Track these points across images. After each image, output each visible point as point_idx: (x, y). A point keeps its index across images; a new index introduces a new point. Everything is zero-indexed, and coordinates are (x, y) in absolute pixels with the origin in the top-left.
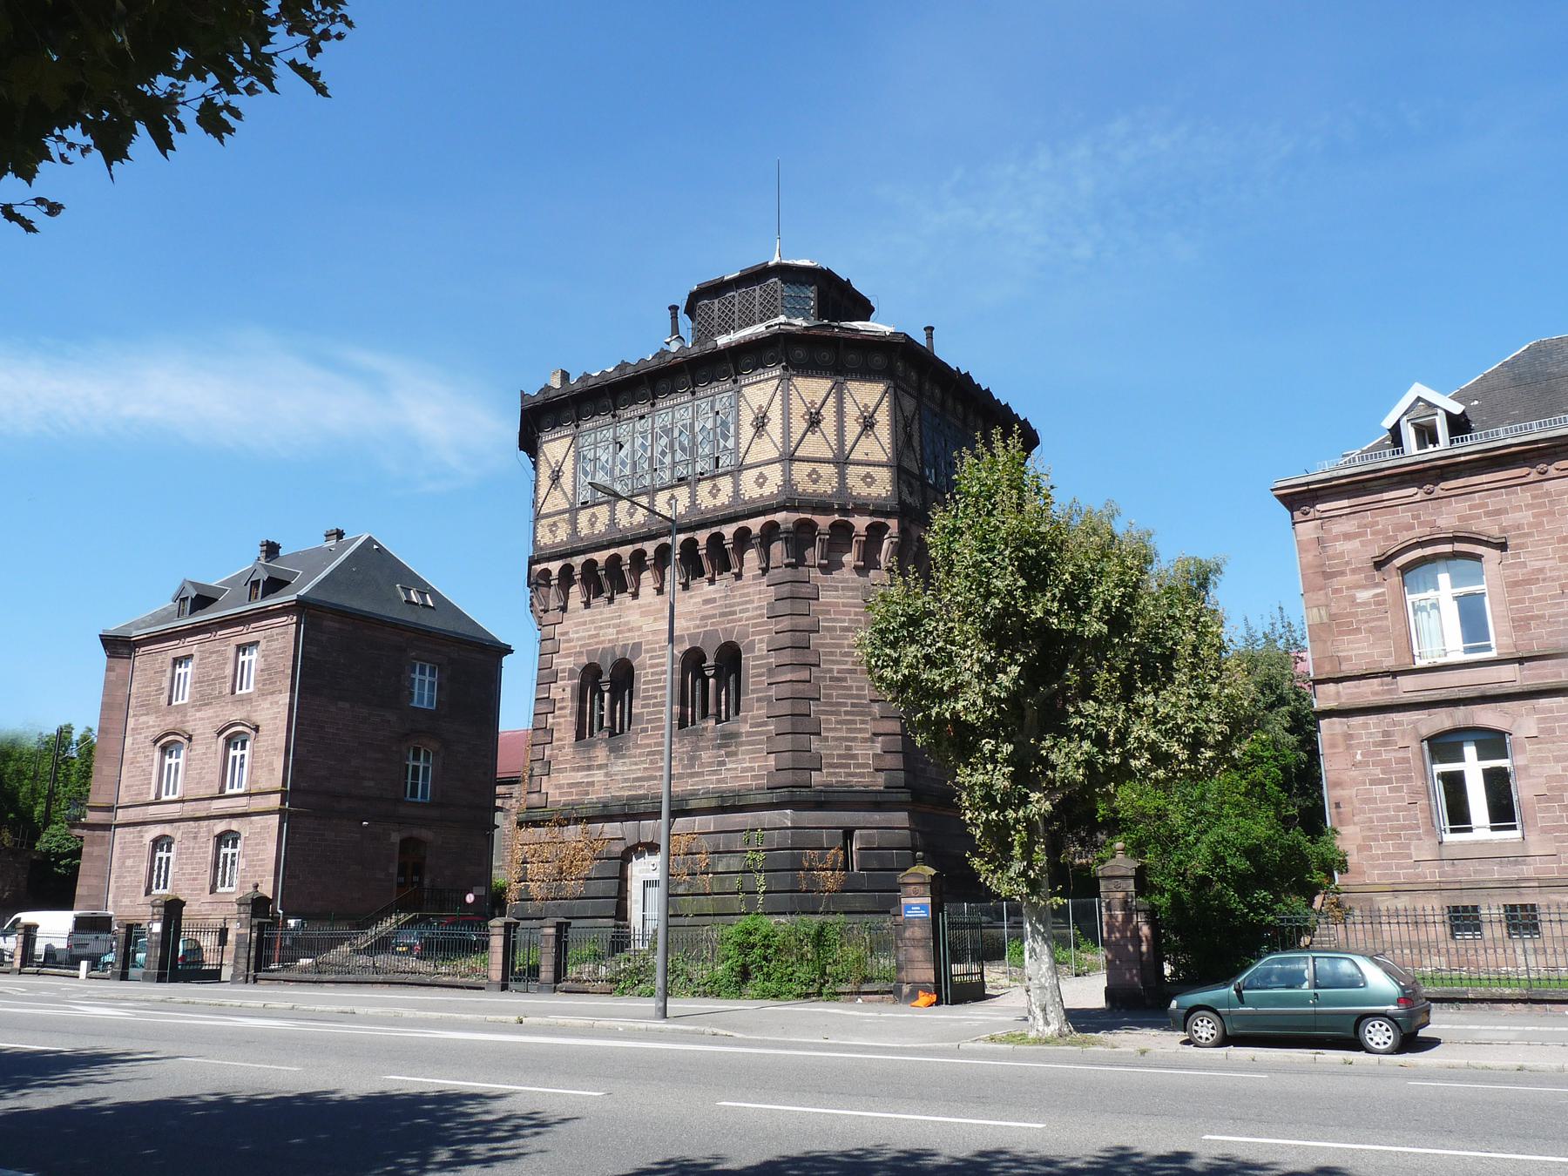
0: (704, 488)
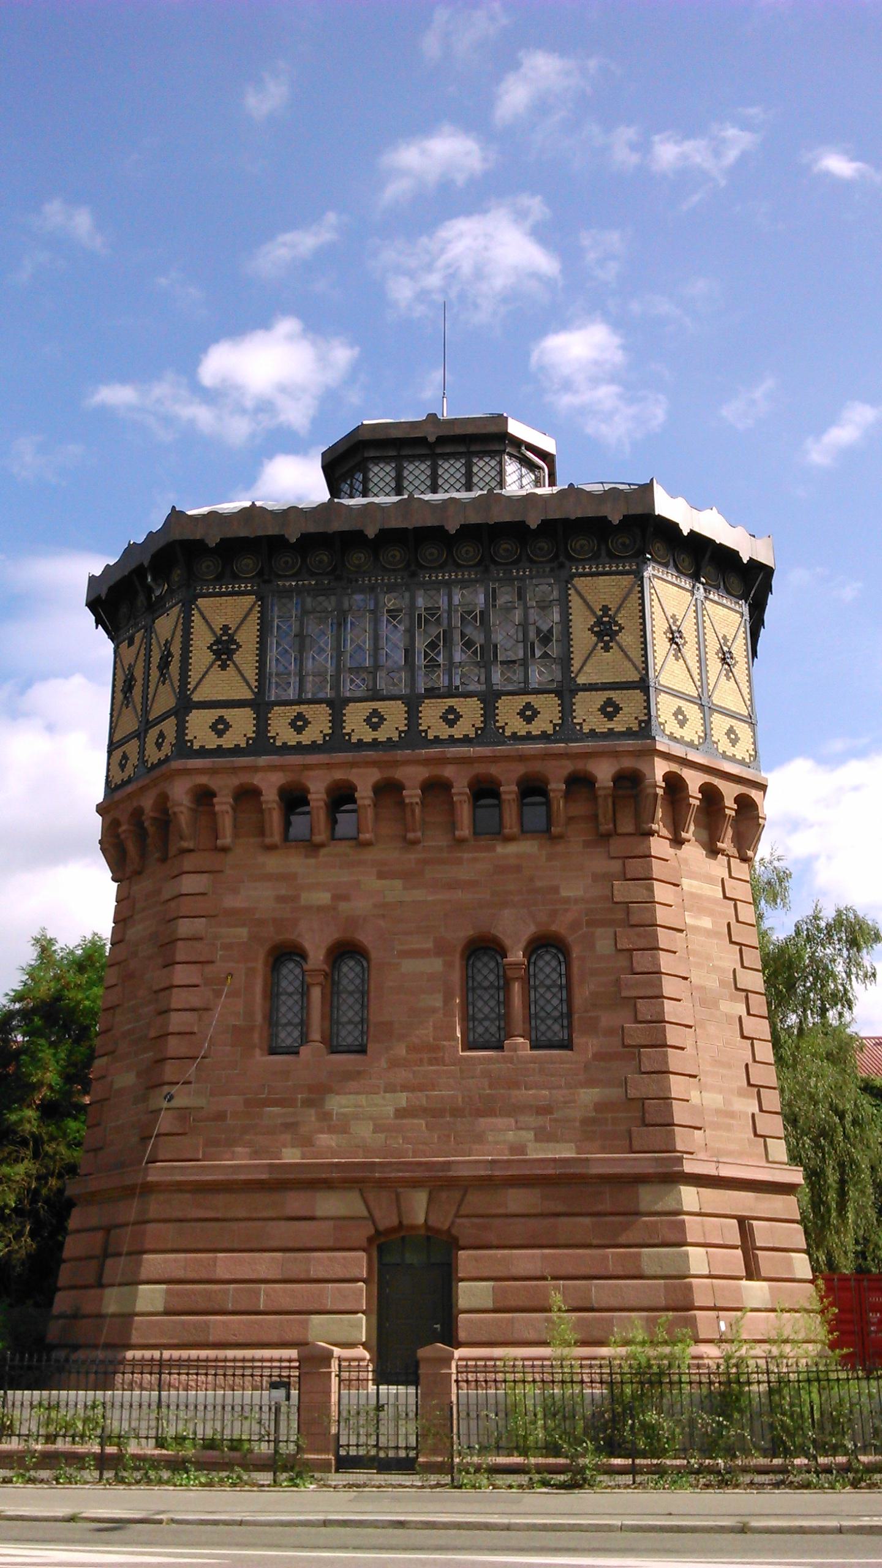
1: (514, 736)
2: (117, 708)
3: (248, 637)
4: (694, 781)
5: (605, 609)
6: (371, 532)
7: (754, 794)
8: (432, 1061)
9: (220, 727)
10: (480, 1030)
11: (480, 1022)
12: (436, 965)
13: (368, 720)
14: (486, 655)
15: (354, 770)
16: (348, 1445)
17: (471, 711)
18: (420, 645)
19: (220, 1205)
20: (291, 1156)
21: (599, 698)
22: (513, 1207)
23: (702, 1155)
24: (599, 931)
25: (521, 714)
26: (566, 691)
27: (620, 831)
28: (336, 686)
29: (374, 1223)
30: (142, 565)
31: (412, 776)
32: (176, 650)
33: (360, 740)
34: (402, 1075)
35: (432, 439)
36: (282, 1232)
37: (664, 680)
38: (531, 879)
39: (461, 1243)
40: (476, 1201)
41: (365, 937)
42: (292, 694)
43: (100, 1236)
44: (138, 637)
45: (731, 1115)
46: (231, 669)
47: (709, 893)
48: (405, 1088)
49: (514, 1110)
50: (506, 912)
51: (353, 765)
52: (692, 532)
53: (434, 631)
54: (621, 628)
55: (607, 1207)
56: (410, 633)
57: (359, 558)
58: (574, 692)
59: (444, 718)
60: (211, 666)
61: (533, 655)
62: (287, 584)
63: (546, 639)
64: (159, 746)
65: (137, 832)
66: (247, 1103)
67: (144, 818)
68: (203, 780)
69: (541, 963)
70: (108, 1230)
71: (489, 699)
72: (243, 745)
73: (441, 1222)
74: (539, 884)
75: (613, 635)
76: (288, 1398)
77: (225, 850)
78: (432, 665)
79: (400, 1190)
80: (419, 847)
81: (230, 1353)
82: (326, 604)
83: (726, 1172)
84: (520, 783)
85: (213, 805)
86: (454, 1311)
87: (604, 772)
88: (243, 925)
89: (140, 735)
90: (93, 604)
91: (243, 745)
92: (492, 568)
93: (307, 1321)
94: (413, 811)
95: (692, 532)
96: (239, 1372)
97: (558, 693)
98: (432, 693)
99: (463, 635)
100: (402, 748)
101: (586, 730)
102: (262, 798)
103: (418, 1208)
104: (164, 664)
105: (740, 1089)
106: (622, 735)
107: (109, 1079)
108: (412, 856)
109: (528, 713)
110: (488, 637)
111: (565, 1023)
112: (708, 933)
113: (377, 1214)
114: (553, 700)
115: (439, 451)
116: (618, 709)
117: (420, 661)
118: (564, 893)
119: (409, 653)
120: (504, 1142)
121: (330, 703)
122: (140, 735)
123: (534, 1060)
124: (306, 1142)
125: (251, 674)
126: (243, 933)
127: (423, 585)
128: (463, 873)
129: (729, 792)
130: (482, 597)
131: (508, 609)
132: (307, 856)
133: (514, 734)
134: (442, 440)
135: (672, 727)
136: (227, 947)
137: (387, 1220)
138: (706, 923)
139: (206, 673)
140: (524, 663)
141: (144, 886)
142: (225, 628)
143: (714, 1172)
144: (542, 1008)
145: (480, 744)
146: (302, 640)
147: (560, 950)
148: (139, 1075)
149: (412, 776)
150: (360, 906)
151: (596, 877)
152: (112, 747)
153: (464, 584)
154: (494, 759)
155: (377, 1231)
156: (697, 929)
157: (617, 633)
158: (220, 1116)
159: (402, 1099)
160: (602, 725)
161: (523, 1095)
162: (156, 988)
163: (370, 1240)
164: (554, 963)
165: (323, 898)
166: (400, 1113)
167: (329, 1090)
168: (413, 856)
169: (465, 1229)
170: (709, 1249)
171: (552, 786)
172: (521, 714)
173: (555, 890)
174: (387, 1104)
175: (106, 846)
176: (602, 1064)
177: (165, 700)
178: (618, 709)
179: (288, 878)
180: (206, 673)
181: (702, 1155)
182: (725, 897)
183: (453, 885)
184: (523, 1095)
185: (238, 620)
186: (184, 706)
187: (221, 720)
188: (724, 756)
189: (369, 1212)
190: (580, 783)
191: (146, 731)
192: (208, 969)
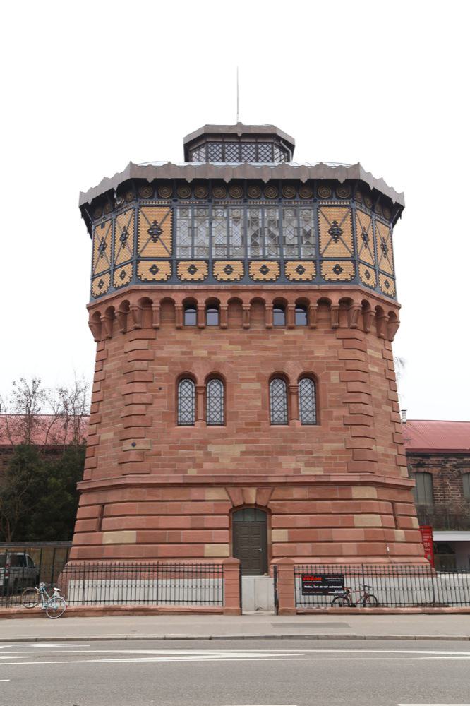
1: (294, 281)
2: (96, 258)
3: (166, 227)
4: (373, 304)
5: (335, 223)
6: (227, 180)
7: (395, 311)
8: (257, 430)
9: (154, 270)
10: (276, 416)
11: (276, 412)
12: (257, 386)
13: (225, 270)
14: (280, 242)
15: (219, 293)
16: (114, 601)
17: (274, 268)
18: (249, 234)
19: (160, 494)
20: (192, 472)
21: (333, 264)
22: (296, 497)
23: (377, 474)
24: (332, 372)
25: (297, 270)
26: (318, 260)
27: (341, 326)
28: (210, 253)
30: (113, 189)
31: (247, 298)
32: (131, 231)
33: (222, 279)
34: (244, 436)
35: (240, 135)
36: (190, 507)
37: (362, 257)
38: (301, 347)
39: (272, 512)
40: (279, 493)
41: (224, 372)
43: (98, 508)
45: (387, 456)
46: (159, 242)
48: (245, 442)
49: (294, 453)
50: (290, 362)
51: (219, 291)
52: (374, 188)
53: (255, 228)
54: (328, 232)
55: (338, 497)
56: (244, 228)
57: (220, 192)
58: (321, 261)
59: (261, 270)
60: (149, 240)
61: (302, 243)
63: (308, 234)
64: (122, 278)
65: (108, 318)
66: (171, 448)
67: (115, 312)
68: (146, 295)
69: (212, 386)
70: (103, 505)
71: (282, 263)
72: (166, 279)
73: (262, 502)
74: (304, 349)
75: (339, 235)
77: (156, 329)
78: (255, 245)
79: (243, 488)
80: (248, 331)
81: (183, 561)
82: (204, 213)
83: (388, 481)
85: (151, 307)
86: (269, 543)
87: (335, 299)
88: (166, 365)
89: (111, 272)
90: (82, 207)
91: (311, 279)
92: (283, 200)
93: (203, 547)
94: (247, 314)
95: (374, 188)
96: (212, 570)
97: (314, 261)
98: (255, 259)
99: (269, 231)
100: (242, 283)
101: (327, 279)
103: (252, 496)
104: (124, 238)
105: (390, 445)
106: (343, 282)
107: (98, 435)
108: (246, 335)
109: (300, 270)
110: (281, 233)
111: (194, 414)
114: (312, 264)
115: (242, 140)
116: (341, 270)
117: (249, 242)
118: (316, 355)
119: (244, 238)
120: (291, 466)
121: (207, 261)
122: (111, 272)
123: (303, 430)
124: (199, 466)
127: (249, 207)
129: (386, 309)
130: (277, 214)
131: (290, 221)
132: (196, 333)
134: (245, 136)
135: (364, 279)
136: (160, 375)
137: (239, 502)
138: (376, 369)
139: (146, 244)
140: (298, 246)
141: (110, 346)
142: (155, 222)
143: (383, 481)
144: (304, 407)
145: (207, 284)
146: (192, 229)
148: (115, 434)
149: (247, 298)
150: (221, 357)
151: (330, 347)
152: (93, 277)
153: (269, 207)
154: (219, 291)
155: (234, 506)
156: (373, 372)
157: (340, 234)
158: (158, 454)
159: (243, 447)
160: (334, 277)
161: (295, 446)
162: (123, 393)
163: (230, 510)
164: (190, 387)
165: (204, 353)
166: (243, 453)
167: (210, 443)
168: (246, 335)
169: (273, 505)
170: (383, 516)
171: (312, 304)
172: (297, 270)
173: (312, 352)
174: (237, 450)
175: (91, 324)
176: (334, 433)
177: (125, 255)
178: (341, 270)
179: (188, 343)
180: (146, 244)
181: (377, 474)
182: (384, 358)
183: (265, 349)
184: (295, 446)
185: (162, 219)
186: (137, 259)
187: (154, 266)
188: (384, 293)
189: (230, 497)
190: (324, 303)
191: (114, 270)
192: (150, 384)
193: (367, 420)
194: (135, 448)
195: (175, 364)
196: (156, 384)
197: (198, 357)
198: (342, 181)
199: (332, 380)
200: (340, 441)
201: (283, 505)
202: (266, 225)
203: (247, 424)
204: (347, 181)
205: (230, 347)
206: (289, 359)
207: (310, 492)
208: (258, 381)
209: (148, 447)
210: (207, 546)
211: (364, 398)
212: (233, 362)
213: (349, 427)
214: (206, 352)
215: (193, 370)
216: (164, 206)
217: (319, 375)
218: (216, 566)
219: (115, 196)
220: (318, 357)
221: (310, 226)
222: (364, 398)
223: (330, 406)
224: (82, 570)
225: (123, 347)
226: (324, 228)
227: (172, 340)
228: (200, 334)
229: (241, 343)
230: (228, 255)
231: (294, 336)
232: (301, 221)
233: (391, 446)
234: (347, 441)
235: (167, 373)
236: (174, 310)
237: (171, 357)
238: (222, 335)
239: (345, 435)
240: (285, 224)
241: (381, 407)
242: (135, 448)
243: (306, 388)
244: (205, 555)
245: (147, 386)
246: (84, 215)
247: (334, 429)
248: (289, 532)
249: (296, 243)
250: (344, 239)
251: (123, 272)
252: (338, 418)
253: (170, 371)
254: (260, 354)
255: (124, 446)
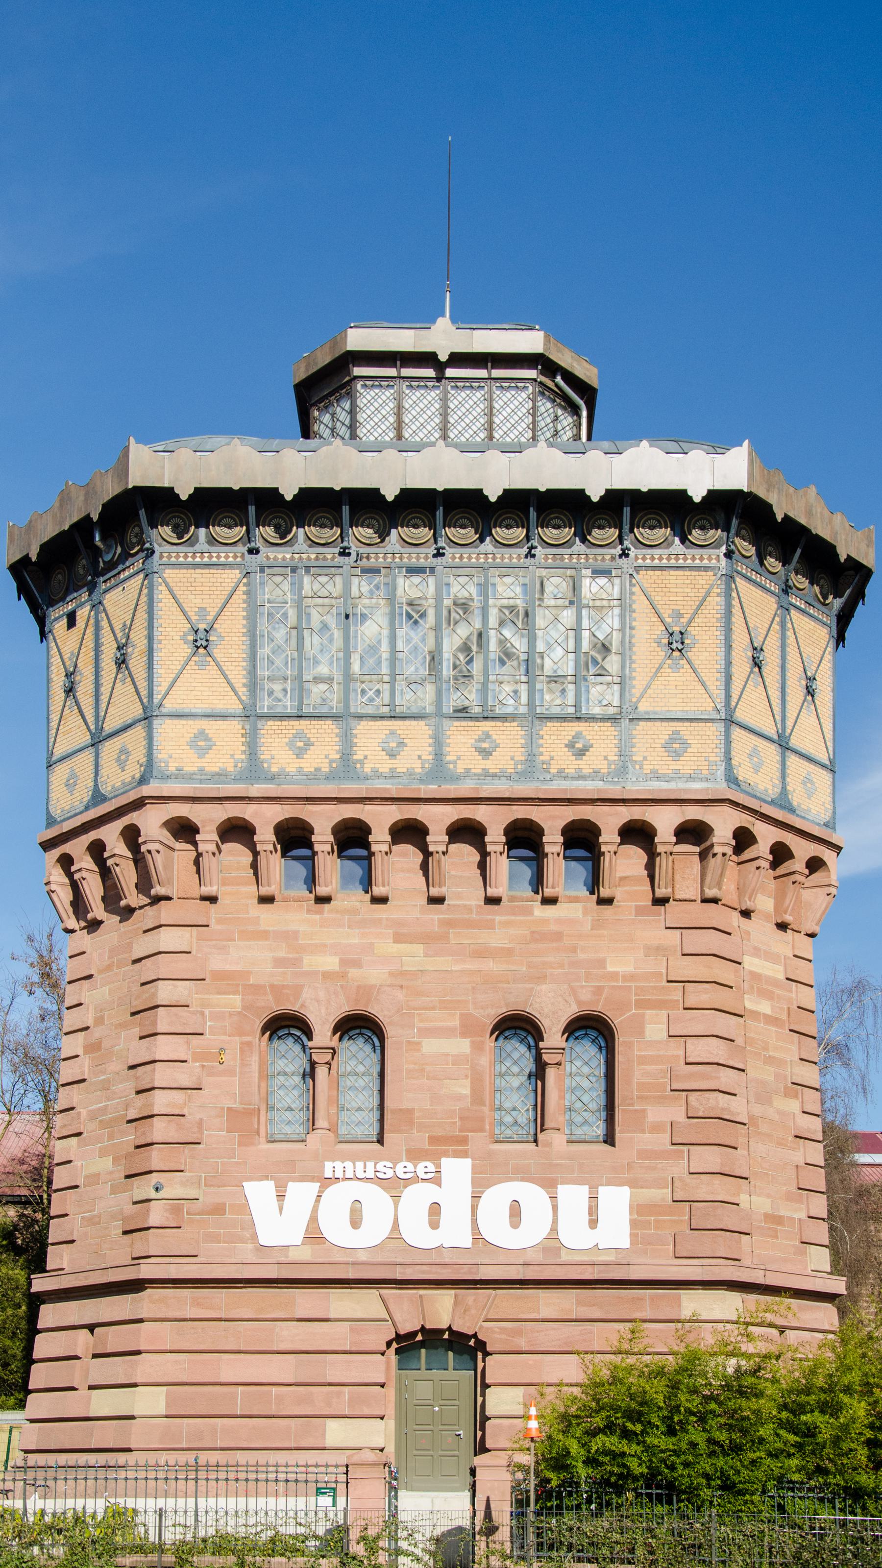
0: (554, 741)
9: (202, 743)
12: (464, 1046)
22: (545, 1313)
29: (394, 1325)
30: (88, 518)
35: (443, 357)
40: (507, 1301)
41: (376, 1010)
42: (288, 705)
44: (83, 614)
45: (778, 1220)
47: (770, 973)
52: (787, 518)
53: (463, 631)
55: (648, 1315)
62: (280, 556)
64: (122, 764)
74: (581, 956)
76: (334, 1504)
82: (329, 587)
84: (508, 831)
88: (235, 993)
95: (787, 518)
102: (256, 838)
112: (770, 1020)
113: (397, 1317)
118: (610, 968)
125: (239, 678)
126: (236, 1001)
128: (496, 939)
133: (561, 771)
138: (765, 1007)
140: (578, 679)
147: (601, 1033)
150: (374, 974)
156: (755, 1015)
165: (331, 963)
173: (602, 963)
179: (289, 937)
183: (481, 953)
193: (737, 1135)
194: (160, 1195)
195: (257, 989)
196: (211, 1041)
197: (316, 973)
198: (697, 494)
199: (647, 1033)
200: (658, 1184)
201: (519, 1333)
202: (493, 621)
203: (433, 1140)
204: (713, 495)
205: (395, 948)
206: (541, 979)
207: (579, 1303)
208: (463, 1035)
209: (191, 1193)
210: (331, 1424)
211: (726, 1079)
212: (401, 987)
213: (685, 1148)
214: (336, 960)
215: (303, 1006)
216: (224, 566)
217: (618, 1021)
218: (331, 1469)
219: (97, 538)
220: (614, 976)
221: (608, 626)
222: (726, 1079)
223: (639, 1097)
224: (192, 1475)
225: (130, 946)
226: (647, 636)
227: (250, 928)
228: (321, 912)
229: (426, 939)
230: (392, 704)
231: (558, 921)
232: (584, 612)
233: (789, 1197)
234: (677, 1183)
235: (239, 1013)
236: (252, 847)
237: (249, 973)
238: (377, 916)
239: (679, 1169)
240: (541, 619)
241: (769, 1102)
242: (160, 1195)
243: (585, 1057)
244: (327, 1445)
245: (188, 1043)
246: (23, 590)
247: (644, 1154)
248: (168, 1395)
249: (571, 671)
250: (696, 663)
251: (124, 751)
252: (656, 1128)
253: (244, 1008)
254: (471, 965)
255: (136, 1190)
